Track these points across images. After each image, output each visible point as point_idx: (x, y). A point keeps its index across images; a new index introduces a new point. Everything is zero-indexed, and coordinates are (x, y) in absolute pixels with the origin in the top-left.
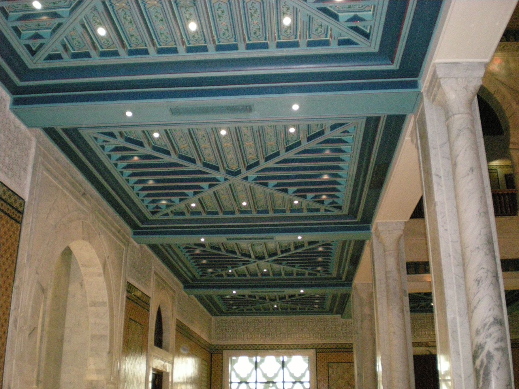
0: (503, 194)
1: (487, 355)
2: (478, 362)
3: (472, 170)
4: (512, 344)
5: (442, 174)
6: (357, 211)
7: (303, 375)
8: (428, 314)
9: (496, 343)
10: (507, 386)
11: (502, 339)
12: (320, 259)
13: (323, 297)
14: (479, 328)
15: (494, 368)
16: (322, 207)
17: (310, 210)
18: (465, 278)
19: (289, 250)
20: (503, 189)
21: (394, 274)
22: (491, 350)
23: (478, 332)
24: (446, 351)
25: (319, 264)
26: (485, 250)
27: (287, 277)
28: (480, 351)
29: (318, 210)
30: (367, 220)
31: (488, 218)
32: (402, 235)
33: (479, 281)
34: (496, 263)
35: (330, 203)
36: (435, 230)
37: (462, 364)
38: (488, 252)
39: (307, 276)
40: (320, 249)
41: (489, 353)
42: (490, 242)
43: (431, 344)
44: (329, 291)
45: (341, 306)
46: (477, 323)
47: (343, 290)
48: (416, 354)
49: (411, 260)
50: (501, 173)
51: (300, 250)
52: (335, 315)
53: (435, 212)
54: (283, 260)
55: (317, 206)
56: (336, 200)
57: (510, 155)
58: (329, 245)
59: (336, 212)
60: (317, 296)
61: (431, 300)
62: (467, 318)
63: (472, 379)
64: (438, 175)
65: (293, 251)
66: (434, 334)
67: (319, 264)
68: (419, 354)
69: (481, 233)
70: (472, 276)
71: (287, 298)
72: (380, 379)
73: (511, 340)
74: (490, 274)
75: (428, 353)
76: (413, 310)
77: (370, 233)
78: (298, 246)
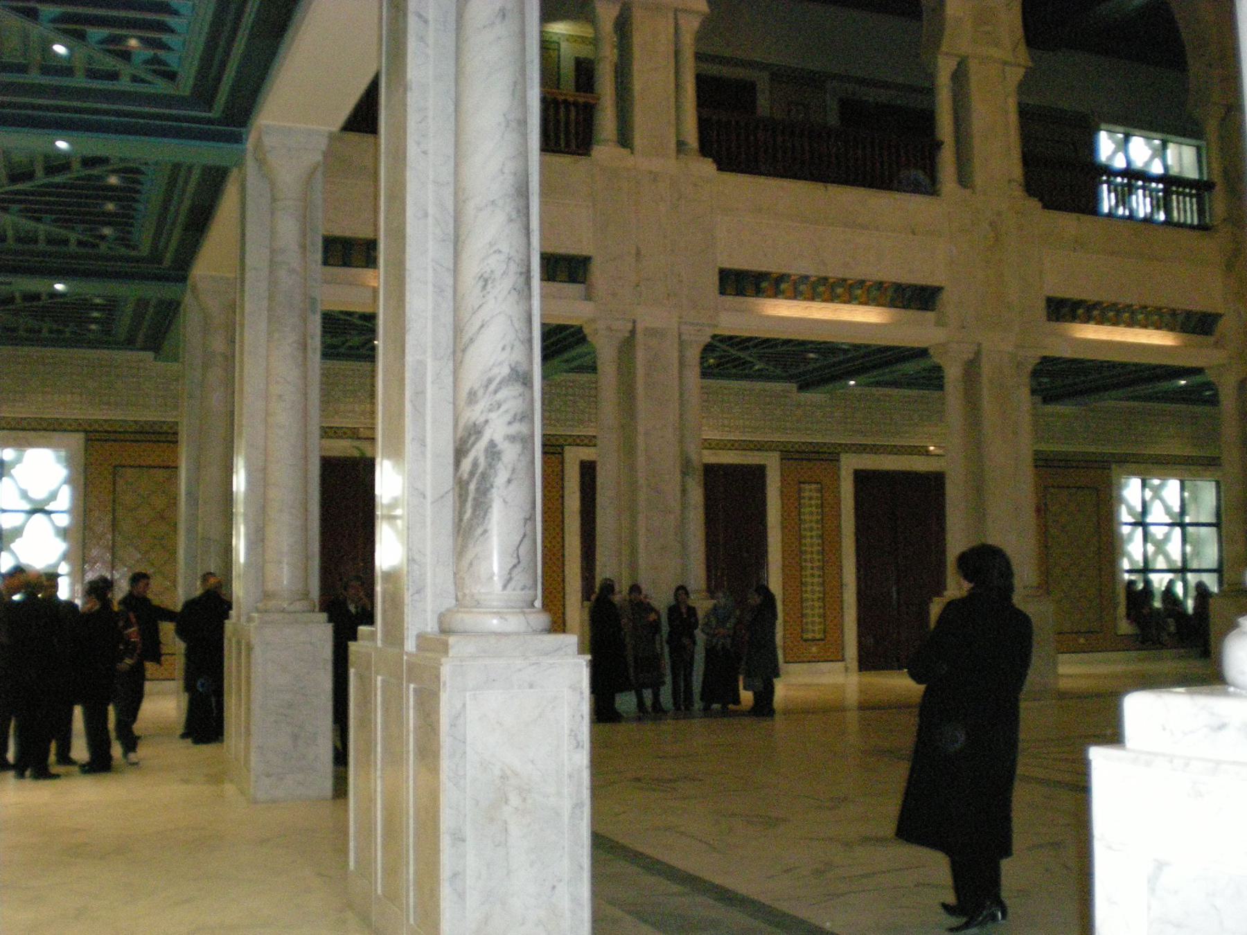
0: (565, 101)
1: (486, 450)
2: (466, 464)
3: (503, 14)
4: (544, 445)
5: (431, 15)
6: (215, 89)
7: (53, 496)
8: (366, 366)
9: (510, 423)
10: (526, 520)
11: (526, 417)
12: (110, 207)
13: (111, 306)
14: (476, 387)
15: (501, 478)
16: (125, 70)
17: (92, 74)
18: (456, 271)
19: (30, 176)
20: (568, 87)
21: (293, 257)
22: (498, 438)
23: (472, 397)
24: (396, 453)
25: (109, 220)
26: (508, 209)
27: (20, 247)
28: (473, 438)
29: (114, 76)
30: (239, 115)
31: (524, 136)
32: (318, 164)
33: (486, 281)
34: (529, 244)
35: (147, 62)
36: (399, 157)
37: (429, 468)
38: (514, 215)
39: (73, 247)
40: (113, 180)
41: (492, 444)
42: (522, 192)
43: (363, 433)
44: (130, 292)
45: (157, 331)
46: (472, 376)
47: (166, 291)
48: (328, 454)
49: (337, 232)
50: (568, 52)
51: (58, 179)
52: (142, 353)
53: (405, 105)
54: (14, 201)
55: (110, 63)
56: (162, 54)
57: (593, 10)
58: (137, 171)
59: (161, 87)
60: (98, 301)
61: (373, 332)
62: (451, 364)
63: (450, 501)
64: (420, 16)
65: (41, 179)
66: (373, 413)
67: (109, 220)
68: (335, 453)
69: (506, 171)
70: (472, 268)
71: (18, 300)
72: (240, 508)
73: (544, 436)
74: (513, 268)
75: (356, 454)
76: (330, 352)
77: (244, 151)
78: (57, 164)
